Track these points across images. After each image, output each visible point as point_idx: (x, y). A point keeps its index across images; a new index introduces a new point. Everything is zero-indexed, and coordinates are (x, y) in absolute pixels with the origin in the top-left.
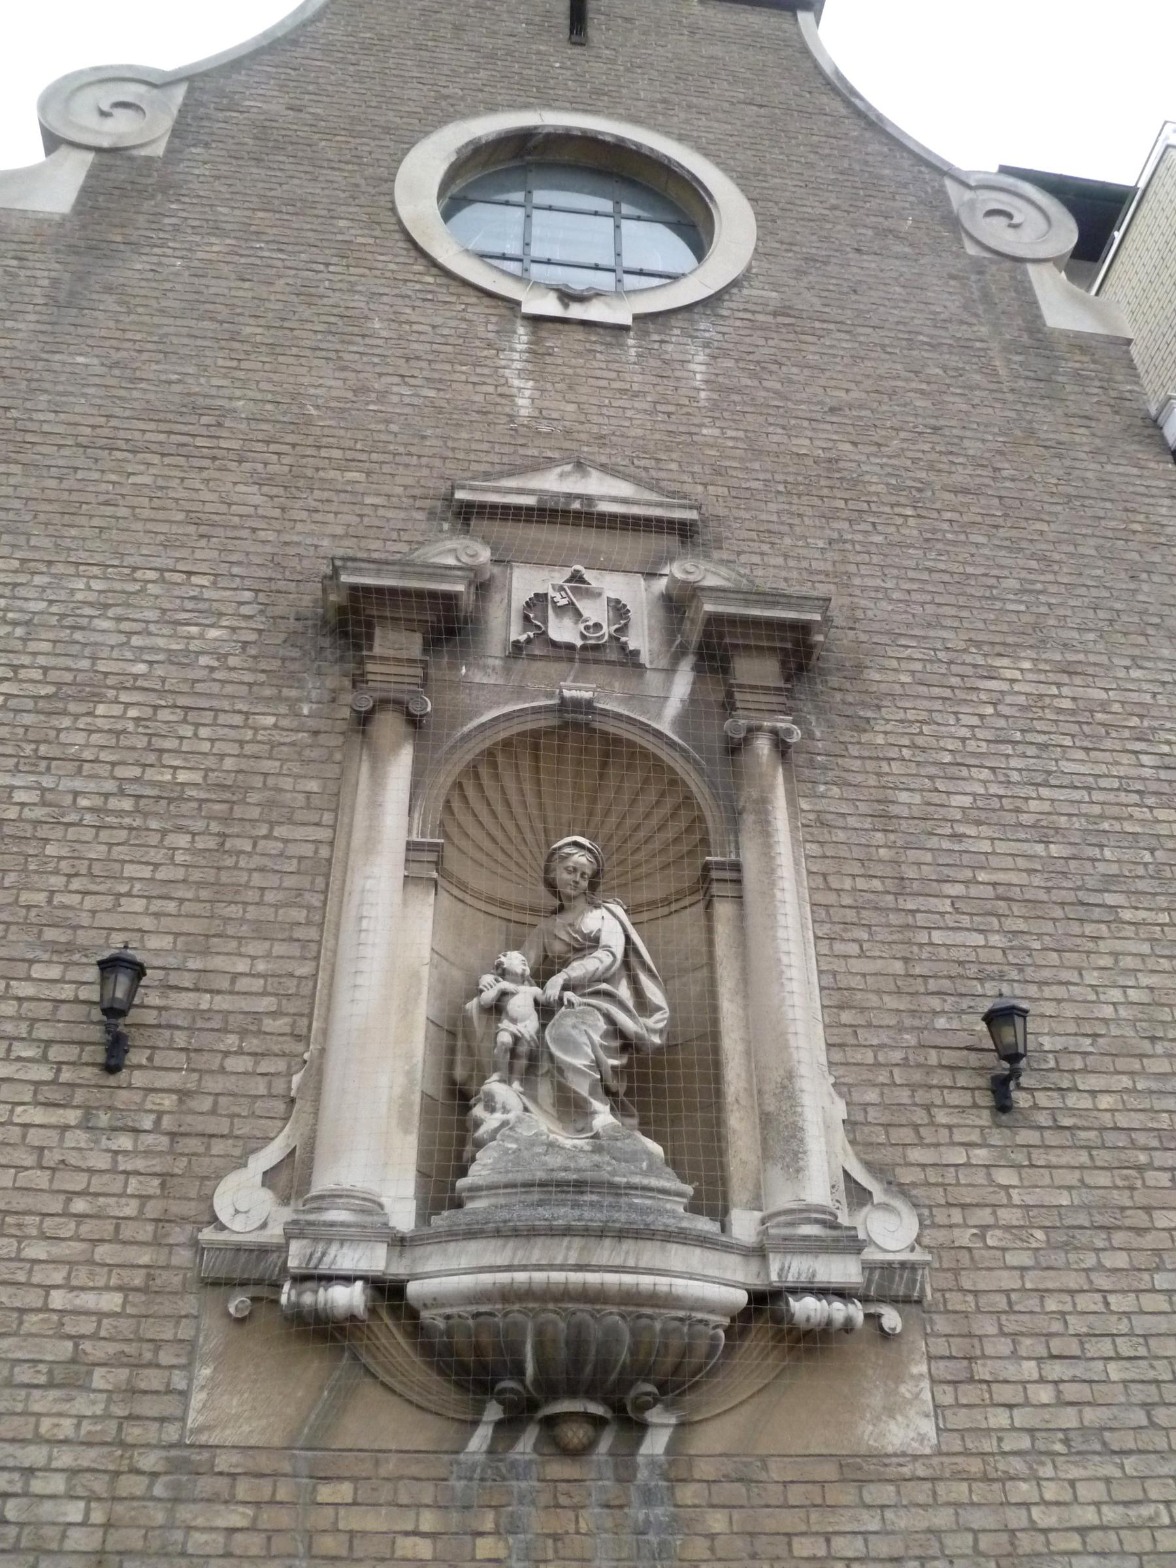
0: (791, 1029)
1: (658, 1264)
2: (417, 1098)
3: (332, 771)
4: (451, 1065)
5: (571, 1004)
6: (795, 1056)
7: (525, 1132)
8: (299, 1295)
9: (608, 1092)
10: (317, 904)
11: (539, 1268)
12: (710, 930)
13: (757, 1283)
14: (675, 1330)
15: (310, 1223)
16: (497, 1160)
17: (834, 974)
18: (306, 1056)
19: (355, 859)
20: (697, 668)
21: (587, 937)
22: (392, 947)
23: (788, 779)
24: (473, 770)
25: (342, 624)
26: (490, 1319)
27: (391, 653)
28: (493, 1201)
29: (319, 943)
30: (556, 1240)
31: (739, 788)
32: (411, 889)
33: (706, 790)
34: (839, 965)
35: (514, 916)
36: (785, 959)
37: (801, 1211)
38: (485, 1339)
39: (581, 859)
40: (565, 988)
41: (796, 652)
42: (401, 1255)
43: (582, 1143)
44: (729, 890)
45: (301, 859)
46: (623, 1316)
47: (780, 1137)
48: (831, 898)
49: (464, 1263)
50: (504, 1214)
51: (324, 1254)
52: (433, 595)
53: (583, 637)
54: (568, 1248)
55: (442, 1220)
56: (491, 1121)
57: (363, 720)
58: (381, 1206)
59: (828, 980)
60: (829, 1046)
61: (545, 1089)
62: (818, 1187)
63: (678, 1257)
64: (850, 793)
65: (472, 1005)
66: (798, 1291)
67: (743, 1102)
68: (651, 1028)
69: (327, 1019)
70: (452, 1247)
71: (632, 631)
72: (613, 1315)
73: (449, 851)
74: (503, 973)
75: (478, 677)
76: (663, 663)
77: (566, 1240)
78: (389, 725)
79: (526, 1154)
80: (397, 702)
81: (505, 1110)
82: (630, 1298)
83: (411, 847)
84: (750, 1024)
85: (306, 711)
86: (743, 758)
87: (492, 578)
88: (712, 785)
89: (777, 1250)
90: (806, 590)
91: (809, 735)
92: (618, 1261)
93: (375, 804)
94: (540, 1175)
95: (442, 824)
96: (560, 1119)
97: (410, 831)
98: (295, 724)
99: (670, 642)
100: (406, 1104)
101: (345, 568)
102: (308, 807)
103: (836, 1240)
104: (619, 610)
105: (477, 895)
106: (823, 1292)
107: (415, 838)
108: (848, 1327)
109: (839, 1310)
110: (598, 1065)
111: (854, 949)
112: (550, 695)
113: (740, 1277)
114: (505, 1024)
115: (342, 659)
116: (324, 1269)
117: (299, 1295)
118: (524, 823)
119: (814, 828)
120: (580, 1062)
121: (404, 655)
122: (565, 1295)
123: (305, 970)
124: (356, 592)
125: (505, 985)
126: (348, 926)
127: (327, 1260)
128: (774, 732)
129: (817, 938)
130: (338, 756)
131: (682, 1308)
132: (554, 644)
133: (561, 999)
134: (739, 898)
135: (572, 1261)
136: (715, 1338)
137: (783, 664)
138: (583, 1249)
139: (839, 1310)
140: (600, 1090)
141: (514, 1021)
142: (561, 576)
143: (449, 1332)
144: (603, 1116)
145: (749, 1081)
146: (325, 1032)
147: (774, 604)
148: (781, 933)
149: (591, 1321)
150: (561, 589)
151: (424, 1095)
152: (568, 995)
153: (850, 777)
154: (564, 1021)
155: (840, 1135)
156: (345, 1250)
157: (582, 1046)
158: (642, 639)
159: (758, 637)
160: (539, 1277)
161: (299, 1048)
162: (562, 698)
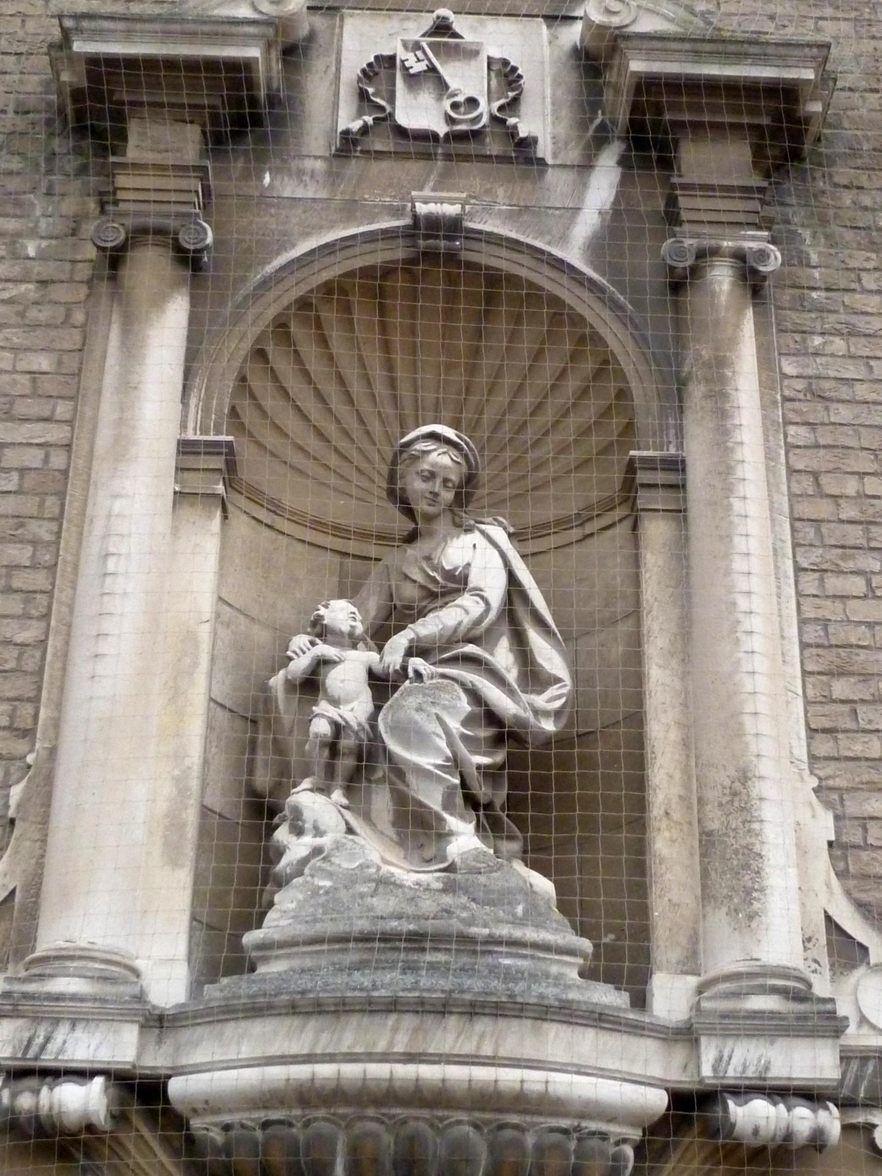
0: (749, 708)
1: (529, 1051)
2: (191, 816)
3: (71, 339)
4: (251, 772)
5: (419, 675)
6: (753, 749)
7: (344, 863)
8: (14, 1096)
9: (472, 801)
10: (47, 537)
11: (351, 1058)
12: (636, 561)
13: (683, 1079)
14: (557, 1147)
15: (26, 996)
16: (301, 905)
17: (825, 623)
18: (30, 759)
19: (100, 469)
20: (624, 162)
21: (449, 575)
22: (156, 598)
23: (761, 328)
24: (280, 328)
25: (79, 115)
26: (283, 1131)
27: (150, 157)
28: (296, 963)
29: (50, 593)
30: (377, 1019)
31: (680, 342)
32: (187, 512)
33: (631, 347)
34: (831, 610)
35: (352, 546)
36: (743, 603)
37: (751, 975)
38: (277, 1158)
39: (441, 458)
40: (410, 652)
41: (775, 133)
42: (160, 1041)
43: (431, 878)
44: (658, 500)
45: (23, 471)
46: (476, 1127)
47: (729, 869)
48: (824, 509)
49: (246, 1051)
50: (305, 982)
51: (48, 1040)
52: (212, 65)
53: (450, 120)
54: (395, 1030)
55: (213, 992)
56: (295, 848)
57: (114, 260)
58: (136, 973)
59: (814, 634)
60: (812, 732)
61: (382, 802)
62: (781, 938)
63: (558, 1041)
64: (861, 347)
65: (277, 681)
66: (744, 1091)
67: (676, 816)
68: (541, 711)
69: (59, 705)
70: (230, 1028)
71: (525, 107)
72: (462, 1125)
73: (246, 453)
74: (321, 631)
75: (289, 189)
76: (573, 155)
77: (392, 1019)
78: (149, 266)
79: (344, 895)
80: (160, 231)
81: (318, 832)
82: (486, 1100)
83: (186, 448)
84: (688, 701)
85: (31, 251)
86: (688, 298)
87: (311, 37)
88: (641, 341)
89: (711, 1032)
90: (790, 33)
91: (796, 258)
92: (468, 1048)
93: (128, 387)
94: (362, 925)
95: (234, 412)
96: (401, 843)
97: (183, 426)
98: (16, 270)
99: (583, 125)
100: (174, 824)
101: (79, 30)
102: (35, 394)
103: (802, 1017)
104: (507, 75)
105: (297, 518)
106: (780, 1093)
107: (190, 435)
108: (818, 1142)
109: (803, 1119)
110: (456, 764)
111: (858, 585)
112: (397, 212)
113: (656, 1071)
114: (323, 707)
115: (82, 171)
116: (48, 1060)
117: (14, 1096)
118: (366, 408)
119: (797, 403)
120: (427, 761)
121: (170, 159)
122: (389, 1096)
123: (29, 634)
124: (101, 68)
125: (324, 649)
126: (89, 568)
127: (52, 1047)
128: (740, 256)
129: (799, 570)
130: (79, 317)
131: (566, 1115)
132: (401, 132)
133: (404, 668)
134: (680, 514)
135: (399, 1048)
136: (618, 1158)
137: (758, 152)
138: (416, 1030)
139: (803, 1119)
140: (459, 800)
141: (335, 702)
142: (416, 27)
143: (227, 1149)
144: (464, 838)
145: (687, 787)
146: (57, 724)
147: (739, 57)
148: (739, 564)
149: (430, 1133)
150: (417, 46)
151: (205, 811)
152: (417, 663)
153: (861, 323)
154: (407, 702)
155: (822, 863)
156: (79, 1033)
157: (434, 736)
158: (541, 121)
159: (715, 109)
160: (351, 1071)
161: (20, 746)
162: (415, 217)
